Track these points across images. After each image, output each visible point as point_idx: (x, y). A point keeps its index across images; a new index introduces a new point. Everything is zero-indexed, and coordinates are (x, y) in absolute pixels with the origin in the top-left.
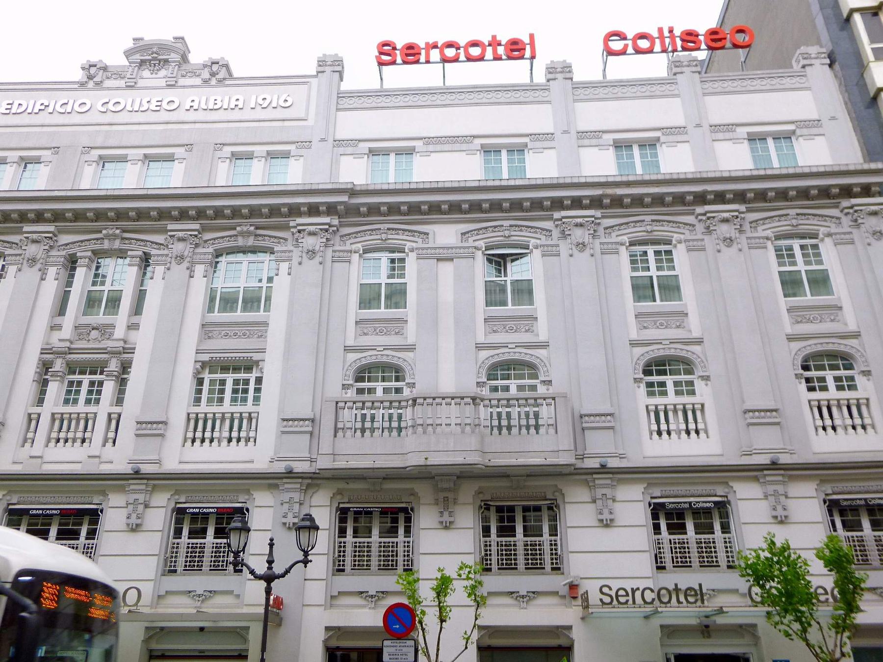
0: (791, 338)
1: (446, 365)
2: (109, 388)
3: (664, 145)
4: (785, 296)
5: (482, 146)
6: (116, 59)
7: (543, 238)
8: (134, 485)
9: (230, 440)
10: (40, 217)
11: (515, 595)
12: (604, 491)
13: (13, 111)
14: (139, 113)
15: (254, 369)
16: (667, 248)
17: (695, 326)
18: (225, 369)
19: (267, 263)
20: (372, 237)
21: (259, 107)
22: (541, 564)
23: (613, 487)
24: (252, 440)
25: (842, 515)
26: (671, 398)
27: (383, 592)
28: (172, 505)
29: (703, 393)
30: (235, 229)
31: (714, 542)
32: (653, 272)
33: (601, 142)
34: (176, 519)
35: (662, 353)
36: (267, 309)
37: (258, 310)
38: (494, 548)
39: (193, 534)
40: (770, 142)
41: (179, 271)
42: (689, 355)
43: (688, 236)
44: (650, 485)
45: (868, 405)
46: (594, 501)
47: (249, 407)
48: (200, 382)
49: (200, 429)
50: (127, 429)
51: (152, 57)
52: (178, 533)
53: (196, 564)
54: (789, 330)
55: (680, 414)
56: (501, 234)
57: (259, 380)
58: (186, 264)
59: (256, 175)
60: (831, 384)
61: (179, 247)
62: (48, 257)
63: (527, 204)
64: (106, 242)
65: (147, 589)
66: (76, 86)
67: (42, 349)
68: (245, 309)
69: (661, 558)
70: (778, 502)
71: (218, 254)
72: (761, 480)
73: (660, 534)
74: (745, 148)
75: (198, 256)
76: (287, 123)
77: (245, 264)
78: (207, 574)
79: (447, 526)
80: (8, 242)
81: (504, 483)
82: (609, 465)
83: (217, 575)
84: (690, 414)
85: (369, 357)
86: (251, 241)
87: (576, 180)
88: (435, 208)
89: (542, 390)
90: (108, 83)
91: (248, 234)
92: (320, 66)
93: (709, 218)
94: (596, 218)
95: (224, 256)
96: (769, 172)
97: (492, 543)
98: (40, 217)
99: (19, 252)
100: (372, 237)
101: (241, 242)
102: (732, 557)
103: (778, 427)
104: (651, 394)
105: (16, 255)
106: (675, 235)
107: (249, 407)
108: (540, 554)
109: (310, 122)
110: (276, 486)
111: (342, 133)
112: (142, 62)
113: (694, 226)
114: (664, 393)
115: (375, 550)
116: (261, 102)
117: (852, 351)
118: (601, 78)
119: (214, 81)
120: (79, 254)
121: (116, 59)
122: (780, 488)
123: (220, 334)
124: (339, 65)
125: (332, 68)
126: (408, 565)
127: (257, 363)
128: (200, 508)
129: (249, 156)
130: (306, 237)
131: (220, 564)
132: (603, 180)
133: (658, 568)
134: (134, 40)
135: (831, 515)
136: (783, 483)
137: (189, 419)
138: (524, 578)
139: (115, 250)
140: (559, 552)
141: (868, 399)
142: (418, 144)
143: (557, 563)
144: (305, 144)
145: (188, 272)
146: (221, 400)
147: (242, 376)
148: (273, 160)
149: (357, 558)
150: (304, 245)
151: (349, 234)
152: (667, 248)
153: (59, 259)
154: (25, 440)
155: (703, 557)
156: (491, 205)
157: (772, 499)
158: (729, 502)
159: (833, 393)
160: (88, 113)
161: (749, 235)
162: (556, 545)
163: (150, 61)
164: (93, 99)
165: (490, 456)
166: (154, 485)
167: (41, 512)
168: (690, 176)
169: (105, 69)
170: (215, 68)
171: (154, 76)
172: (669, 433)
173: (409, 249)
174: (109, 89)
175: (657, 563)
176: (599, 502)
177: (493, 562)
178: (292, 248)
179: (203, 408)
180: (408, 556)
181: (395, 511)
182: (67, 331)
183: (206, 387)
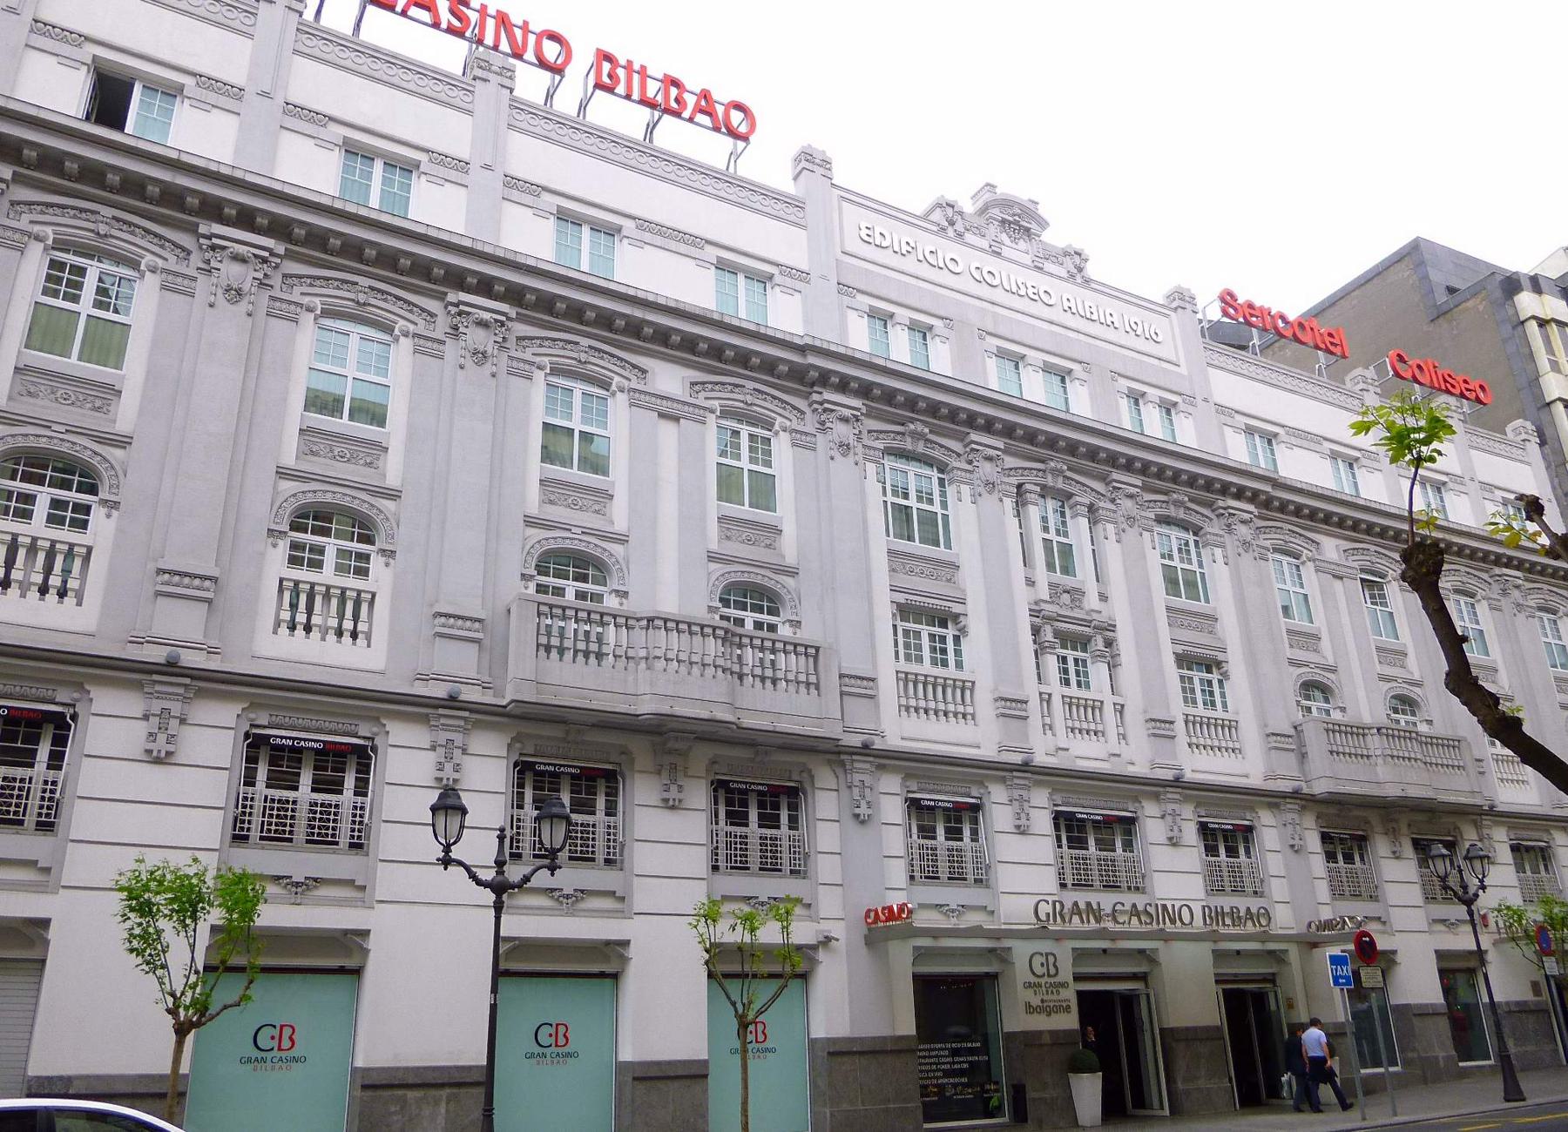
0: (712, 557)
1: (667, 572)
3: (626, 241)
4: (720, 499)
7: (421, 322)
8: (1172, 794)
9: (43, 590)
11: (753, 902)
12: (862, 777)
15: (950, 625)
16: (766, 433)
17: (393, 471)
20: (562, 352)
22: (333, 836)
23: (1028, 788)
26: (327, 575)
27: (315, 880)
28: (515, 757)
29: (380, 575)
32: (745, 463)
35: (43, 443)
40: (378, 166)
42: (778, 588)
43: (795, 425)
44: (1055, 791)
45: (372, 603)
51: (1017, 220)
54: (714, 546)
56: (741, 397)
60: (330, 558)
63: (648, 331)
69: (243, 822)
70: (449, 758)
74: (335, 158)
78: (725, 874)
79: (671, 806)
81: (556, 732)
82: (462, 697)
84: (350, 606)
85: (329, 496)
88: (662, 336)
89: (785, 631)
93: (825, 410)
96: (363, 212)
100: (562, 352)
101: (908, 444)
103: (476, 646)
104: (294, 561)
106: (402, 322)
108: (335, 821)
112: (1003, 221)
113: (803, 413)
114: (317, 565)
117: (783, 592)
126: (48, 815)
127: (956, 617)
128: (294, 739)
131: (12, 809)
132: (631, 292)
133: (235, 837)
136: (466, 732)
137: (281, 590)
138: (755, 880)
140: (366, 820)
141: (374, 595)
142: (628, 226)
152: (766, 433)
156: (308, 234)
157: (1169, 818)
158: (374, 749)
159: (37, 525)
161: (277, 293)
162: (362, 808)
165: (739, 713)
172: (354, 635)
173: (148, 266)
176: (1169, 818)
177: (253, 826)
181: (775, 792)
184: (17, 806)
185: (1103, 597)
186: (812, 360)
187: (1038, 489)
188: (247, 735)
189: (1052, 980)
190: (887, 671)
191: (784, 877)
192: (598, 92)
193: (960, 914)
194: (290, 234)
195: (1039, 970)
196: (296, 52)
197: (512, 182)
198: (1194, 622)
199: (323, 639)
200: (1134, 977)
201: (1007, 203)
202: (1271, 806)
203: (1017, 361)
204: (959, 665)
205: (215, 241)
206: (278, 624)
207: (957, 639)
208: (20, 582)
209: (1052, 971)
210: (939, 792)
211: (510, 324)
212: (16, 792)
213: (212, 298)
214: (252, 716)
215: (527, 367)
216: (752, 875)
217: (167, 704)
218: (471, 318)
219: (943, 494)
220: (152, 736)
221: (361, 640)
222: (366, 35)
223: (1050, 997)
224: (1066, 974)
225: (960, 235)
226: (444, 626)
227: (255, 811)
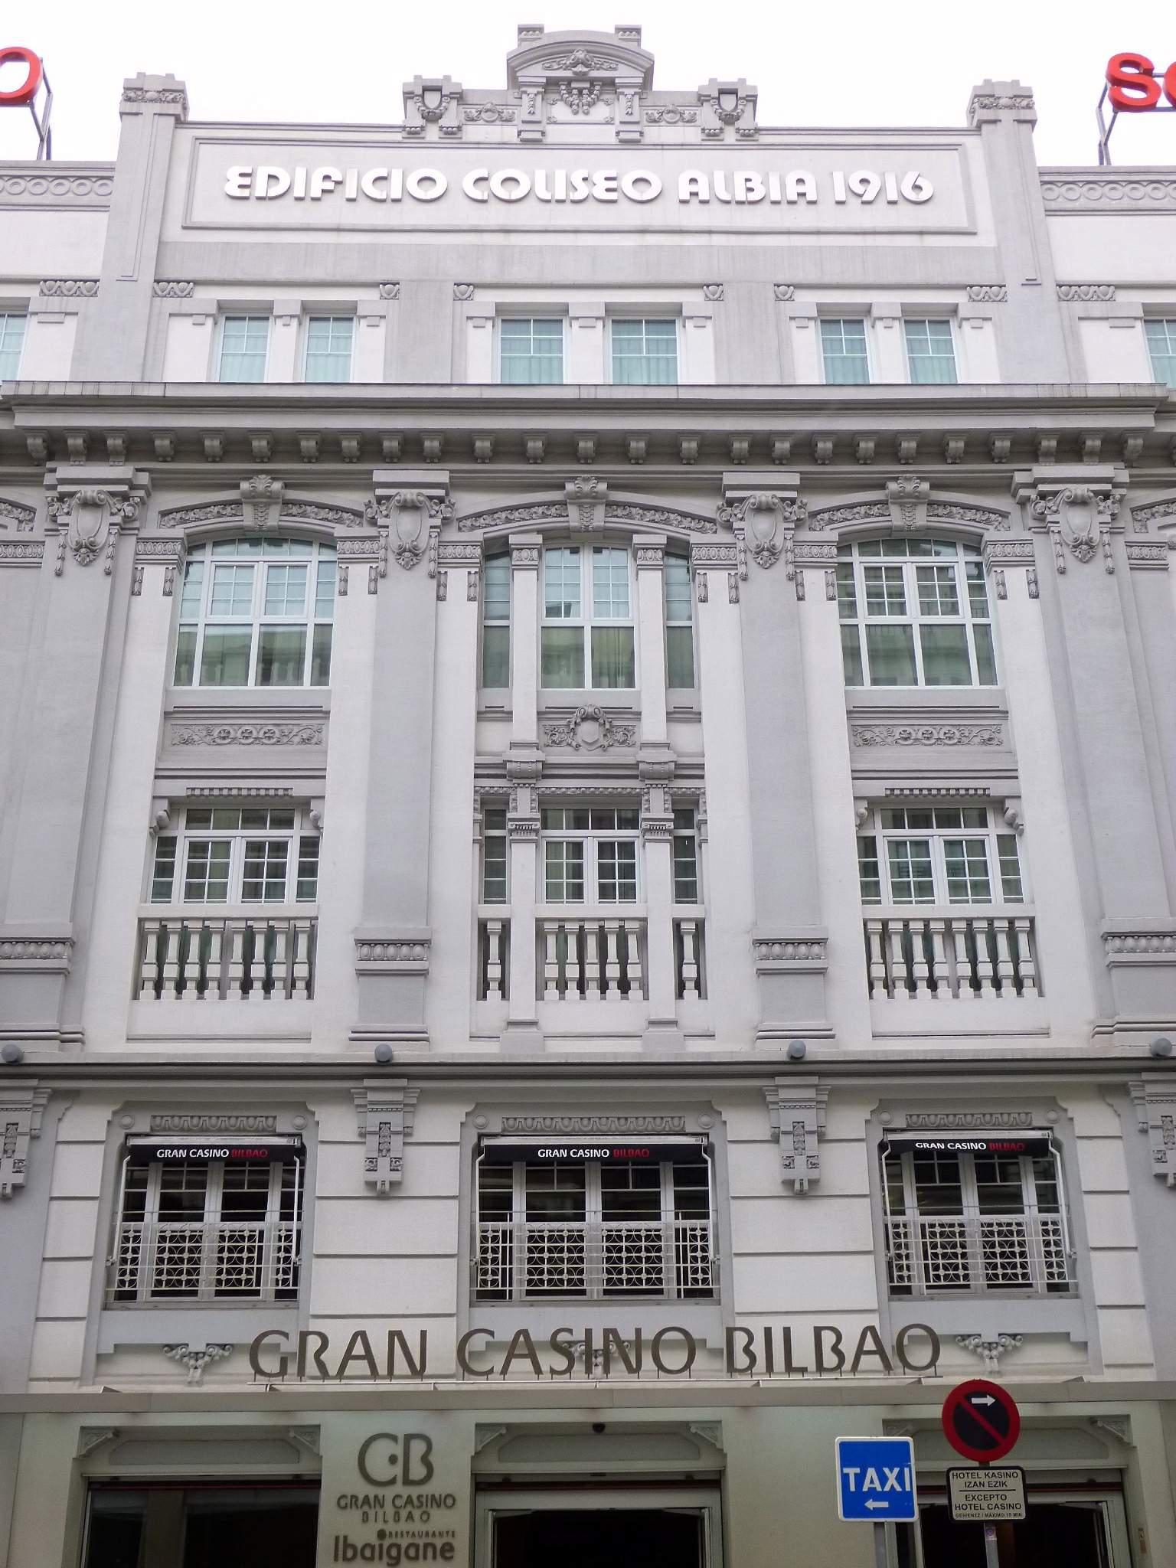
2: (654, 862)
5: (821, 308)
6: (484, 72)
8: (790, 1090)
9: (246, 985)
10: (411, 449)
13: (260, 191)
14: (568, 206)
15: (990, 818)
18: (921, 820)
19: (312, 569)
21: (855, 202)
23: (408, 1108)
24: (300, 985)
25: (532, 1178)
28: (878, 1137)
30: (563, 487)
31: (1020, 1233)
32: (914, 616)
33: (187, 305)
34: (130, 1173)
36: (322, 673)
37: (298, 678)
38: (915, 1242)
39: (171, 1208)
41: (767, 583)
45: (1031, 933)
46: (775, 1139)
47: (289, 904)
48: (165, 846)
49: (170, 959)
50: (729, 960)
51: (579, 72)
52: (134, 1207)
53: (184, 1277)
55: (961, 942)
57: (310, 846)
58: (782, 569)
59: (281, 359)
61: (758, 528)
62: (442, 544)
63: (956, 445)
64: (573, 512)
65: (443, 1340)
66: (398, 137)
67: (477, 766)
68: (208, 678)
69: (900, 1268)
70: (799, 1148)
71: (194, 544)
72: (1134, 1094)
73: (903, 1213)
75: (806, 550)
76: (930, 241)
77: (261, 570)
80: (331, 508)
83: (1009, 1297)
84: (981, 942)
86: (274, 518)
87: (1077, 393)
90: (474, 132)
91: (594, 499)
92: (129, 99)
93: (1043, 496)
94: (1116, 485)
95: (209, 549)
97: (911, 1230)
98: (761, 450)
99: (372, 531)
102: (1059, 1266)
105: (363, 539)
107: (289, 904)
108: (964, 1255)
109: (986, 239)
110: (1123, 1090)
111: (1071, 269)
112: (551, 84)
115: (209, 1247)
116: (859, 189)
118: (1093, 161)
119: (730, 136)
120: (512, 539)
121: (484, 72)
122: (810, 1118)
123: (209, 733)
124: (174, 101)
125: (157, 107)
126: (494, 1282)
127: (304, 804)
129: (262, 314)
130: (394, 513)
132: (1113, 393)
134: (521, 30)
135: (895, 1176)
139: (596, 530)
140: (711, 1254)
141: (1032, 920)
143: (705, 1281)
144: (992, 291)
145: (434, 582)
146: (926, 890)
147: (268, 834)
148: (315, 324)
149: (165, 1267)
150: (1062, 527)
151: (1151, 506)
153: (469, 550)
154: (484, 986)
155: (995, 1267)
156: (598, 445)
158: (710, 1149)
160: (441, 204)
163: (569, 81)
164: (451, 170)
166: (422, 1091)
167: (183, 1153)
168: (56, 391)
169: (460, 97)
170: (432, 100)
171: (581, 117)
172: (932, 984)
174: (478, 145)
175: (891, 1280)
176: (787, 1141)
178: (1027, 535)
179: (178, 906)
180: (287, 1259)
182: (525, 725)
183: (181, 859)
184: (249, 1272)
185: (683, 715)
186: (24, 420)
187: (539, 539)
188: (882, 1146)
189: (414, 1491)
190: (844, 917)
191: (667, 1302)
192: (1122, 115)
193: (1006, 1353)
194: (299, 451)
195: (380, 1468)
196: (1051, 212)
197: (1069, 290)
198: (919, 726)
199: (956, 996)
200: (688, 1482)
201: (559, 49)
202: (1105, 1092)
203: (855, 319)
204: (1012, 888)
205: (1042, 487)
206: (138, 986)
207: (1007, 844)
208: (285, 980)
209: (417, 1471)
210: (204, 1131)
211: (1118, 493)
212: (245, 1255)
213: (1061, 562)
214: (127, 1120)
215: (1155, 551)
216: (976, 1296)
217: (385, 1117)
218: (747, 505)
219: (977, 590)
220: (372, 1164)
221: (1029, 991)
222: (1122, 156)
223: (403, 1526)
224: (454, 1474)
225: (451, 133)
226: (1119, 951)
227: (912, 1251)
